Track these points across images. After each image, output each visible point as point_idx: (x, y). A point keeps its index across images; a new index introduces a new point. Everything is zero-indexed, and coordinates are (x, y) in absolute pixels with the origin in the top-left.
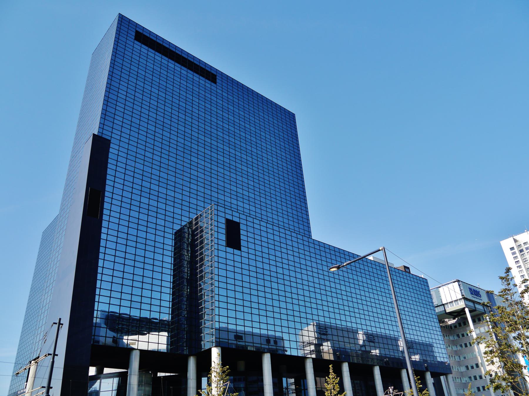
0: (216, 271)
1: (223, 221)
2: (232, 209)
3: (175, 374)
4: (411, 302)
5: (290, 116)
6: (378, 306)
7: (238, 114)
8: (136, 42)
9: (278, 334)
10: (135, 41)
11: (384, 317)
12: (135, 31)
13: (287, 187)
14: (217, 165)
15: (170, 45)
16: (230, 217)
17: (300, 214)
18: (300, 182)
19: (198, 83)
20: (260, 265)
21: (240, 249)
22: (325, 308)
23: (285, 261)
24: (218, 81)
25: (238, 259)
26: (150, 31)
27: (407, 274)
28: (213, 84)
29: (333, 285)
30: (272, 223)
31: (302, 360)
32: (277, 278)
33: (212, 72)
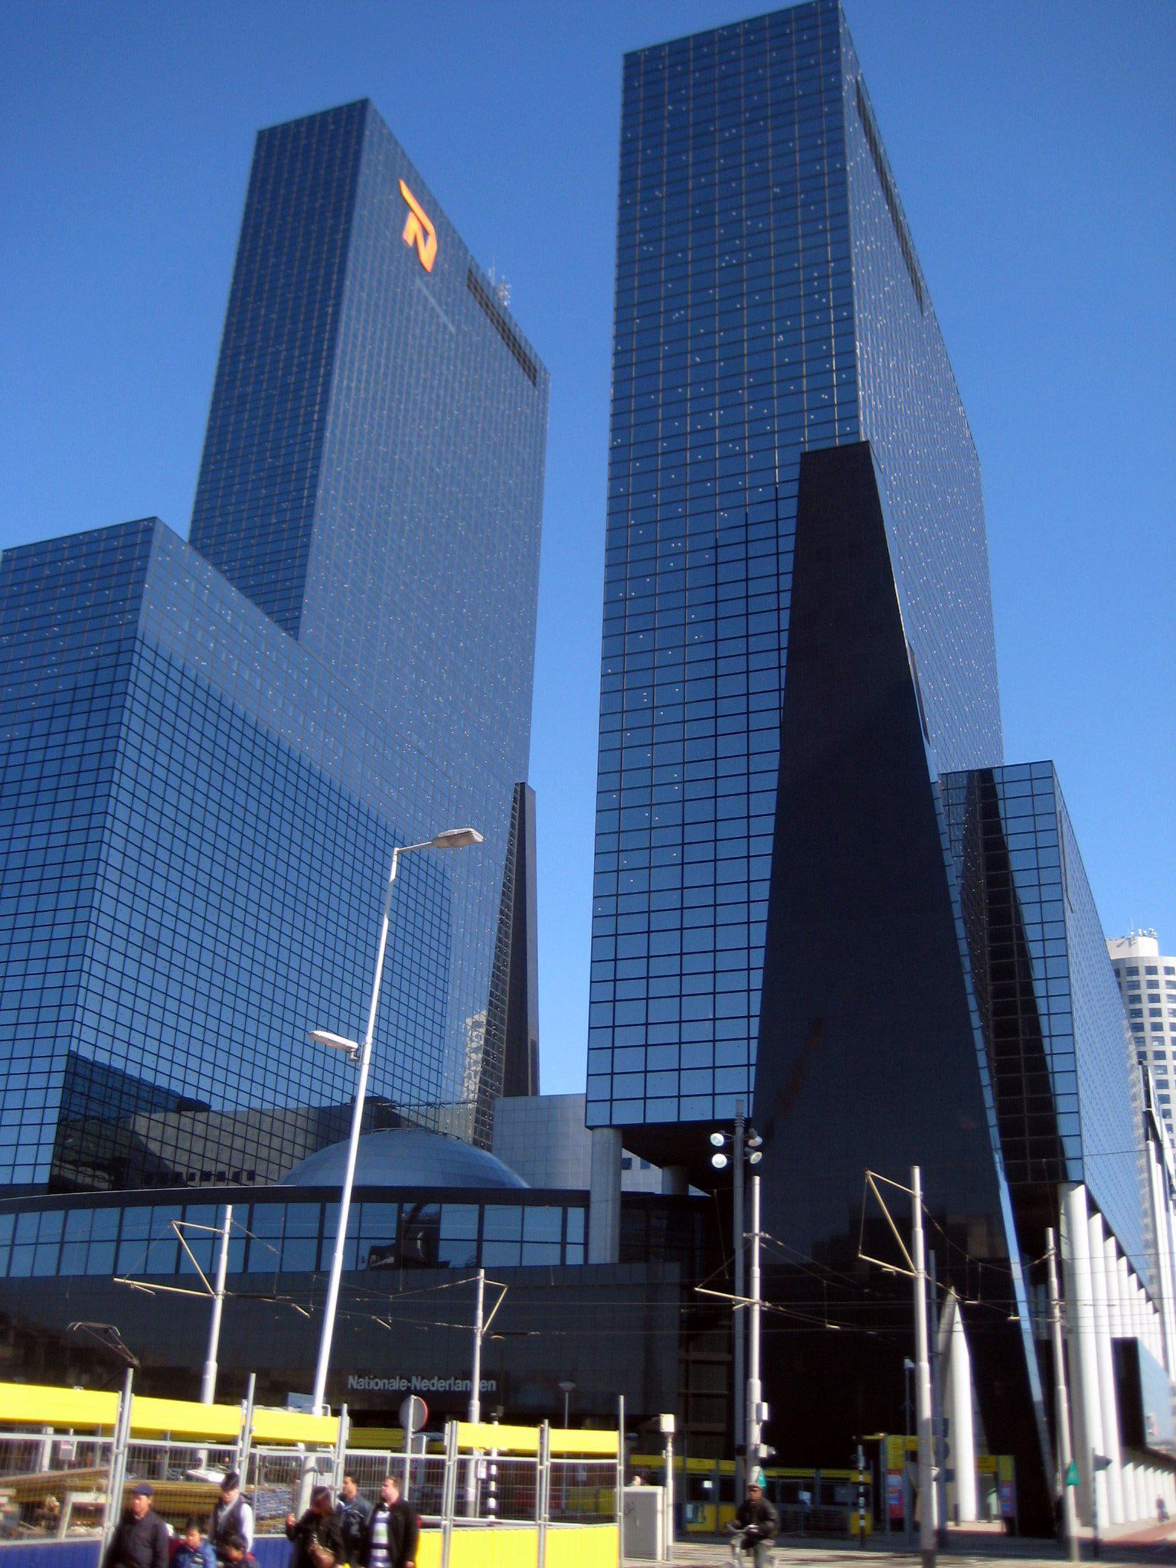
29: (293, 875)
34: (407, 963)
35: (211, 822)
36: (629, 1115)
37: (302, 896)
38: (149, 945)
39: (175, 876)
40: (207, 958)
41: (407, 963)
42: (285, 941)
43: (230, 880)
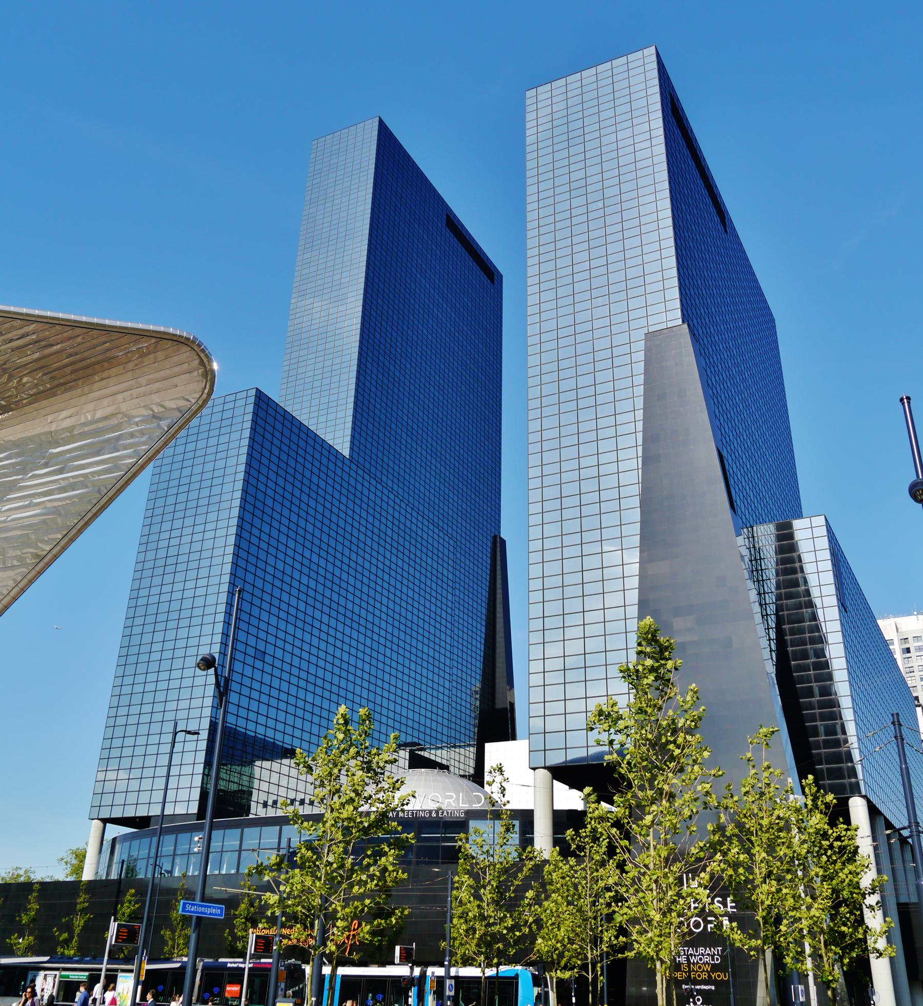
4: (427, 619)
32: (276, 637)
34: (425, 657)
36: (557, 759)
38: (259, 655)
40: (296, 661)
41: (425, 657)
42: (346, 648)
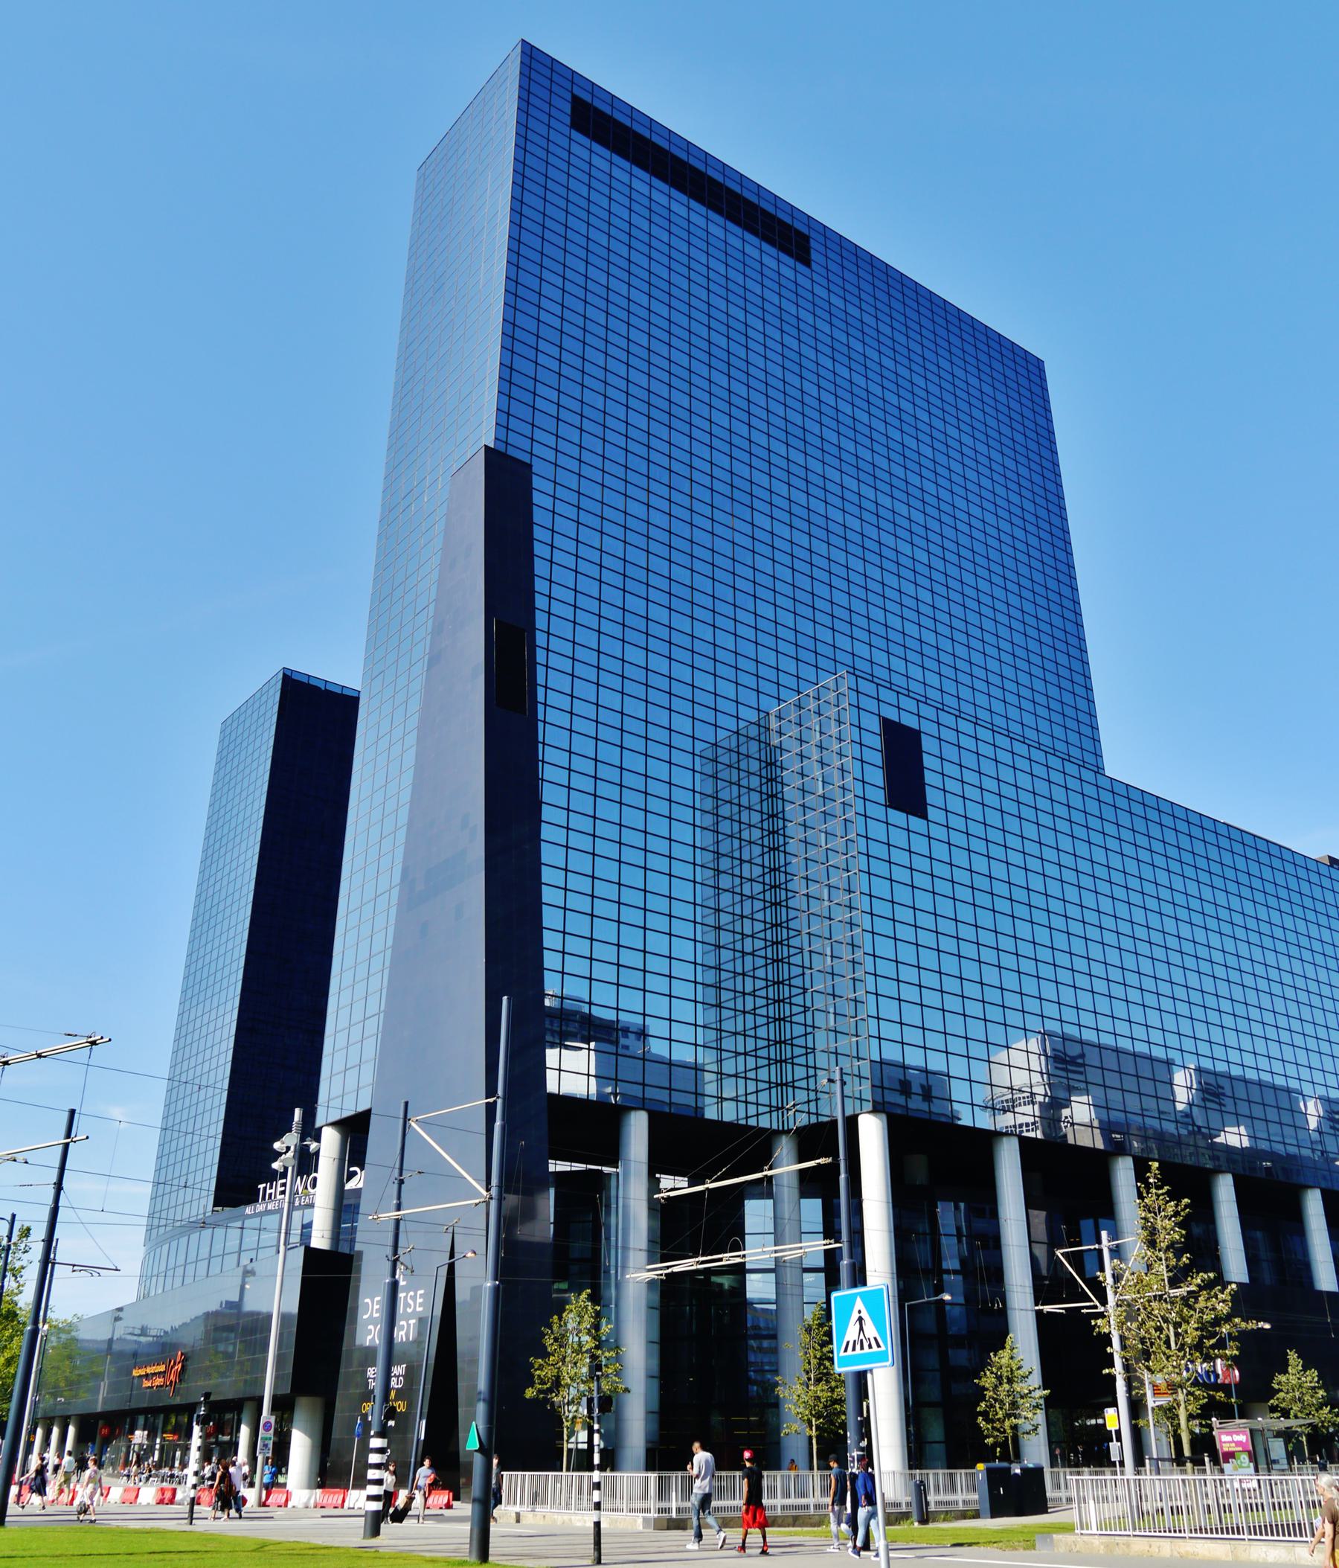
0: (861, 883)
1: (875, 725)
2: (1011, 735)
3: (578, 1167)
5: (1031, 367)
6: (1263, 985)
7: (777, 311)
8: (575, 135)
9: (937, 1063)
10: (573, 131)
11: (1282, 1022)
12: (569, 97)
13: (1029, 607)
14: (689, 476)
15: (779, 204)
16: (892, 714)
17: (1068, 698)
18: (1066, 591)
19: (586, 167)
20: (980, 864)
21: (924, 816)
22: (1082, 981)
23: (1014, 842)
24: (814, 255)
25: (920, 844)
26: (533, 46)
27: (1088, 775)
28: (800, 267)
29: (1185, 931)
30: (974, 720)
31: (986, 1141)
33: (764, 205)
35: (1072, 894)
37: (1211, 1001)
39: (1082, 981)
43: (1130, 961)
